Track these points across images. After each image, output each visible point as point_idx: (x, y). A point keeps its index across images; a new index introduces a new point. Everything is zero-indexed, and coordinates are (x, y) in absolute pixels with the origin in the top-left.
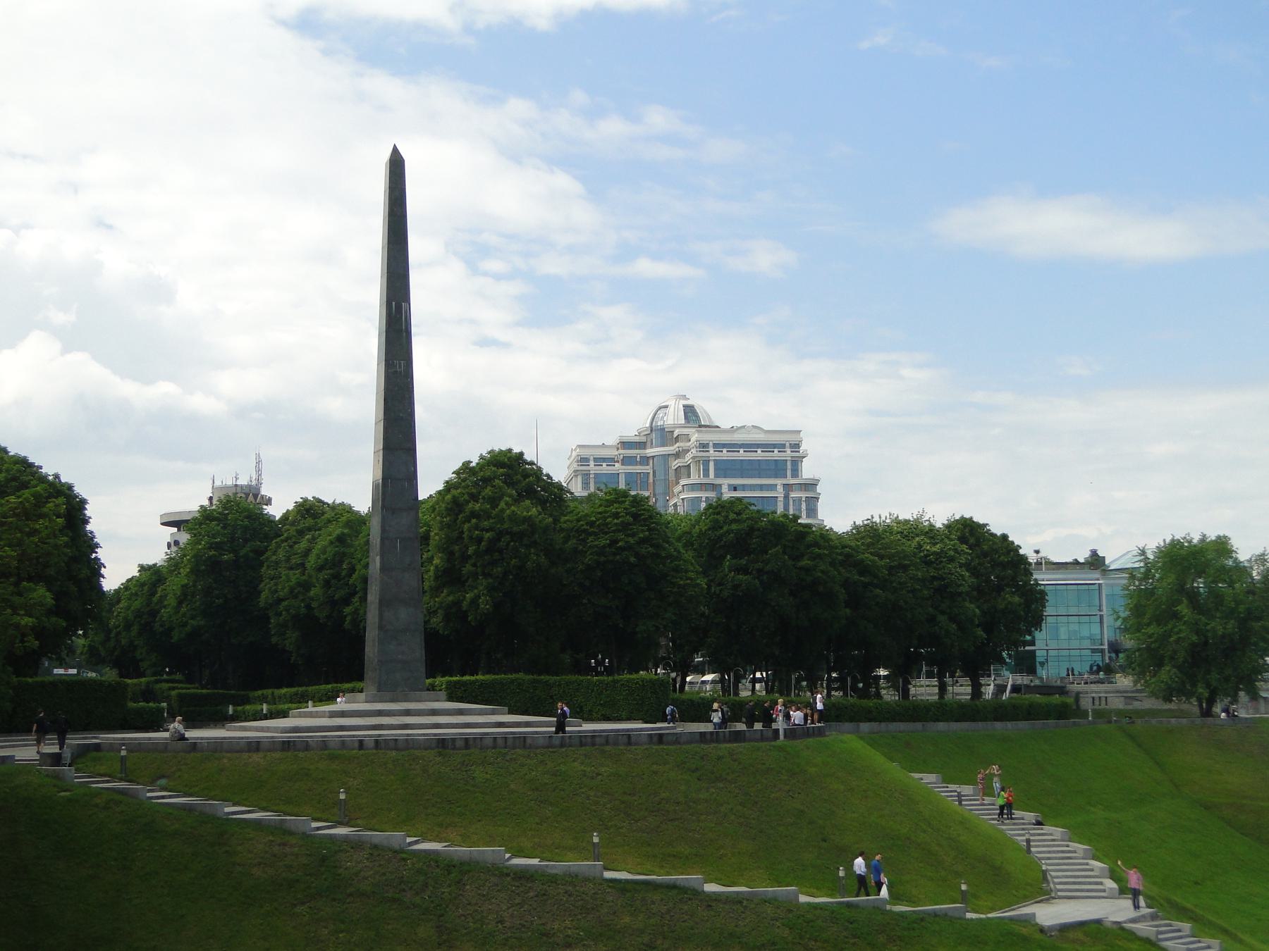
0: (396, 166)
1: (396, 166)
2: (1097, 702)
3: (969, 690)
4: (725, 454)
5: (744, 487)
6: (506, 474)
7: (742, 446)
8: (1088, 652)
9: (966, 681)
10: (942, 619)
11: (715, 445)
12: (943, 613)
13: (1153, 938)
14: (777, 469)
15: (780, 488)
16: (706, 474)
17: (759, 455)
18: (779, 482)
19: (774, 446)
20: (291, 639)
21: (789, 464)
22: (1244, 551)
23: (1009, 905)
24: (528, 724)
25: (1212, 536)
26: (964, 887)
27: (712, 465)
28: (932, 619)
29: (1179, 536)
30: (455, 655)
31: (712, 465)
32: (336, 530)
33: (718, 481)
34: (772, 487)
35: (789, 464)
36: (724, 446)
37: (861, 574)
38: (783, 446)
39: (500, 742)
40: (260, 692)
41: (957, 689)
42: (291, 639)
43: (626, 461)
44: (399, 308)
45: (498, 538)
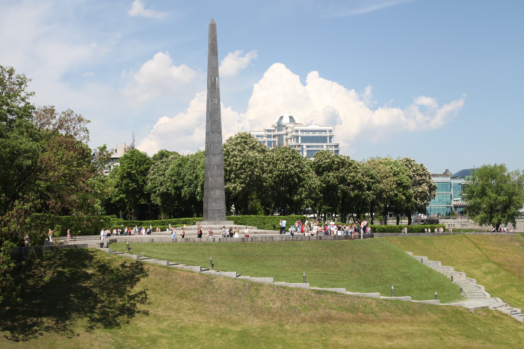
0: (213, 28)
1: (213, 28)
2: (450, 226)
3: (407, 221)
4: (305, 134)
5: (312, 146)
6: (244, 140)
7: (312, 131)
8: (445, 208)
9: (59, 234)
10: (400, 194)
11: (301, 131)
12: (400, 192)
13: (509, 314)
14: (324, 139)
15: (325, 147)
16: (297, 141)
17: (317, 134)
18: (325, 144)
19: (323, 131)
20: (158, 201)
21: (328, 138)
22: (510, 169)
23: (450, 300)
24: (265, 233)
25: (499, 164)
26: (436, 293)
27: (300, 138)
28: (396, 195)
29: (486, 164)
30: (239, 205)
31: (300, 138)
32: (176, 162)
33: (302, 144)
34: (323, 146)
35: (328, 138)
36: (304, 131)
37: (371, 179)
38: (326, 131)
39: (264, 239)
40: (183, 219)
41: (403, 221)
42: (158, 201)
43: (269, 136)
44: (215, 80)
45: (244, 164)
